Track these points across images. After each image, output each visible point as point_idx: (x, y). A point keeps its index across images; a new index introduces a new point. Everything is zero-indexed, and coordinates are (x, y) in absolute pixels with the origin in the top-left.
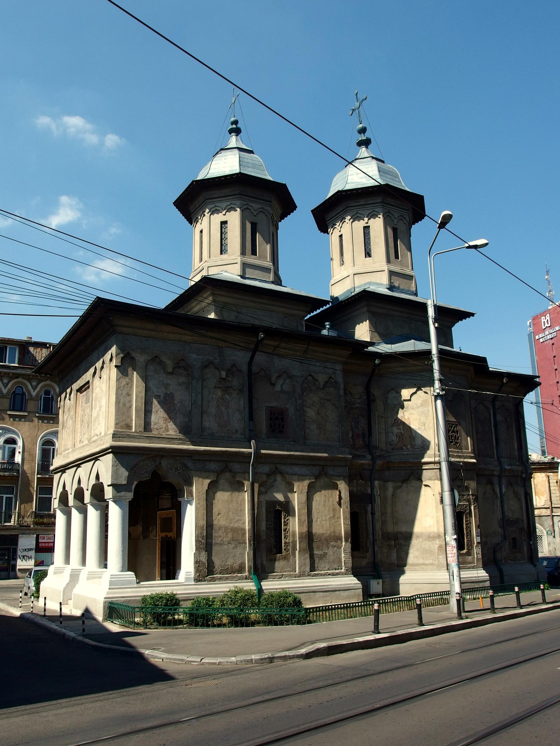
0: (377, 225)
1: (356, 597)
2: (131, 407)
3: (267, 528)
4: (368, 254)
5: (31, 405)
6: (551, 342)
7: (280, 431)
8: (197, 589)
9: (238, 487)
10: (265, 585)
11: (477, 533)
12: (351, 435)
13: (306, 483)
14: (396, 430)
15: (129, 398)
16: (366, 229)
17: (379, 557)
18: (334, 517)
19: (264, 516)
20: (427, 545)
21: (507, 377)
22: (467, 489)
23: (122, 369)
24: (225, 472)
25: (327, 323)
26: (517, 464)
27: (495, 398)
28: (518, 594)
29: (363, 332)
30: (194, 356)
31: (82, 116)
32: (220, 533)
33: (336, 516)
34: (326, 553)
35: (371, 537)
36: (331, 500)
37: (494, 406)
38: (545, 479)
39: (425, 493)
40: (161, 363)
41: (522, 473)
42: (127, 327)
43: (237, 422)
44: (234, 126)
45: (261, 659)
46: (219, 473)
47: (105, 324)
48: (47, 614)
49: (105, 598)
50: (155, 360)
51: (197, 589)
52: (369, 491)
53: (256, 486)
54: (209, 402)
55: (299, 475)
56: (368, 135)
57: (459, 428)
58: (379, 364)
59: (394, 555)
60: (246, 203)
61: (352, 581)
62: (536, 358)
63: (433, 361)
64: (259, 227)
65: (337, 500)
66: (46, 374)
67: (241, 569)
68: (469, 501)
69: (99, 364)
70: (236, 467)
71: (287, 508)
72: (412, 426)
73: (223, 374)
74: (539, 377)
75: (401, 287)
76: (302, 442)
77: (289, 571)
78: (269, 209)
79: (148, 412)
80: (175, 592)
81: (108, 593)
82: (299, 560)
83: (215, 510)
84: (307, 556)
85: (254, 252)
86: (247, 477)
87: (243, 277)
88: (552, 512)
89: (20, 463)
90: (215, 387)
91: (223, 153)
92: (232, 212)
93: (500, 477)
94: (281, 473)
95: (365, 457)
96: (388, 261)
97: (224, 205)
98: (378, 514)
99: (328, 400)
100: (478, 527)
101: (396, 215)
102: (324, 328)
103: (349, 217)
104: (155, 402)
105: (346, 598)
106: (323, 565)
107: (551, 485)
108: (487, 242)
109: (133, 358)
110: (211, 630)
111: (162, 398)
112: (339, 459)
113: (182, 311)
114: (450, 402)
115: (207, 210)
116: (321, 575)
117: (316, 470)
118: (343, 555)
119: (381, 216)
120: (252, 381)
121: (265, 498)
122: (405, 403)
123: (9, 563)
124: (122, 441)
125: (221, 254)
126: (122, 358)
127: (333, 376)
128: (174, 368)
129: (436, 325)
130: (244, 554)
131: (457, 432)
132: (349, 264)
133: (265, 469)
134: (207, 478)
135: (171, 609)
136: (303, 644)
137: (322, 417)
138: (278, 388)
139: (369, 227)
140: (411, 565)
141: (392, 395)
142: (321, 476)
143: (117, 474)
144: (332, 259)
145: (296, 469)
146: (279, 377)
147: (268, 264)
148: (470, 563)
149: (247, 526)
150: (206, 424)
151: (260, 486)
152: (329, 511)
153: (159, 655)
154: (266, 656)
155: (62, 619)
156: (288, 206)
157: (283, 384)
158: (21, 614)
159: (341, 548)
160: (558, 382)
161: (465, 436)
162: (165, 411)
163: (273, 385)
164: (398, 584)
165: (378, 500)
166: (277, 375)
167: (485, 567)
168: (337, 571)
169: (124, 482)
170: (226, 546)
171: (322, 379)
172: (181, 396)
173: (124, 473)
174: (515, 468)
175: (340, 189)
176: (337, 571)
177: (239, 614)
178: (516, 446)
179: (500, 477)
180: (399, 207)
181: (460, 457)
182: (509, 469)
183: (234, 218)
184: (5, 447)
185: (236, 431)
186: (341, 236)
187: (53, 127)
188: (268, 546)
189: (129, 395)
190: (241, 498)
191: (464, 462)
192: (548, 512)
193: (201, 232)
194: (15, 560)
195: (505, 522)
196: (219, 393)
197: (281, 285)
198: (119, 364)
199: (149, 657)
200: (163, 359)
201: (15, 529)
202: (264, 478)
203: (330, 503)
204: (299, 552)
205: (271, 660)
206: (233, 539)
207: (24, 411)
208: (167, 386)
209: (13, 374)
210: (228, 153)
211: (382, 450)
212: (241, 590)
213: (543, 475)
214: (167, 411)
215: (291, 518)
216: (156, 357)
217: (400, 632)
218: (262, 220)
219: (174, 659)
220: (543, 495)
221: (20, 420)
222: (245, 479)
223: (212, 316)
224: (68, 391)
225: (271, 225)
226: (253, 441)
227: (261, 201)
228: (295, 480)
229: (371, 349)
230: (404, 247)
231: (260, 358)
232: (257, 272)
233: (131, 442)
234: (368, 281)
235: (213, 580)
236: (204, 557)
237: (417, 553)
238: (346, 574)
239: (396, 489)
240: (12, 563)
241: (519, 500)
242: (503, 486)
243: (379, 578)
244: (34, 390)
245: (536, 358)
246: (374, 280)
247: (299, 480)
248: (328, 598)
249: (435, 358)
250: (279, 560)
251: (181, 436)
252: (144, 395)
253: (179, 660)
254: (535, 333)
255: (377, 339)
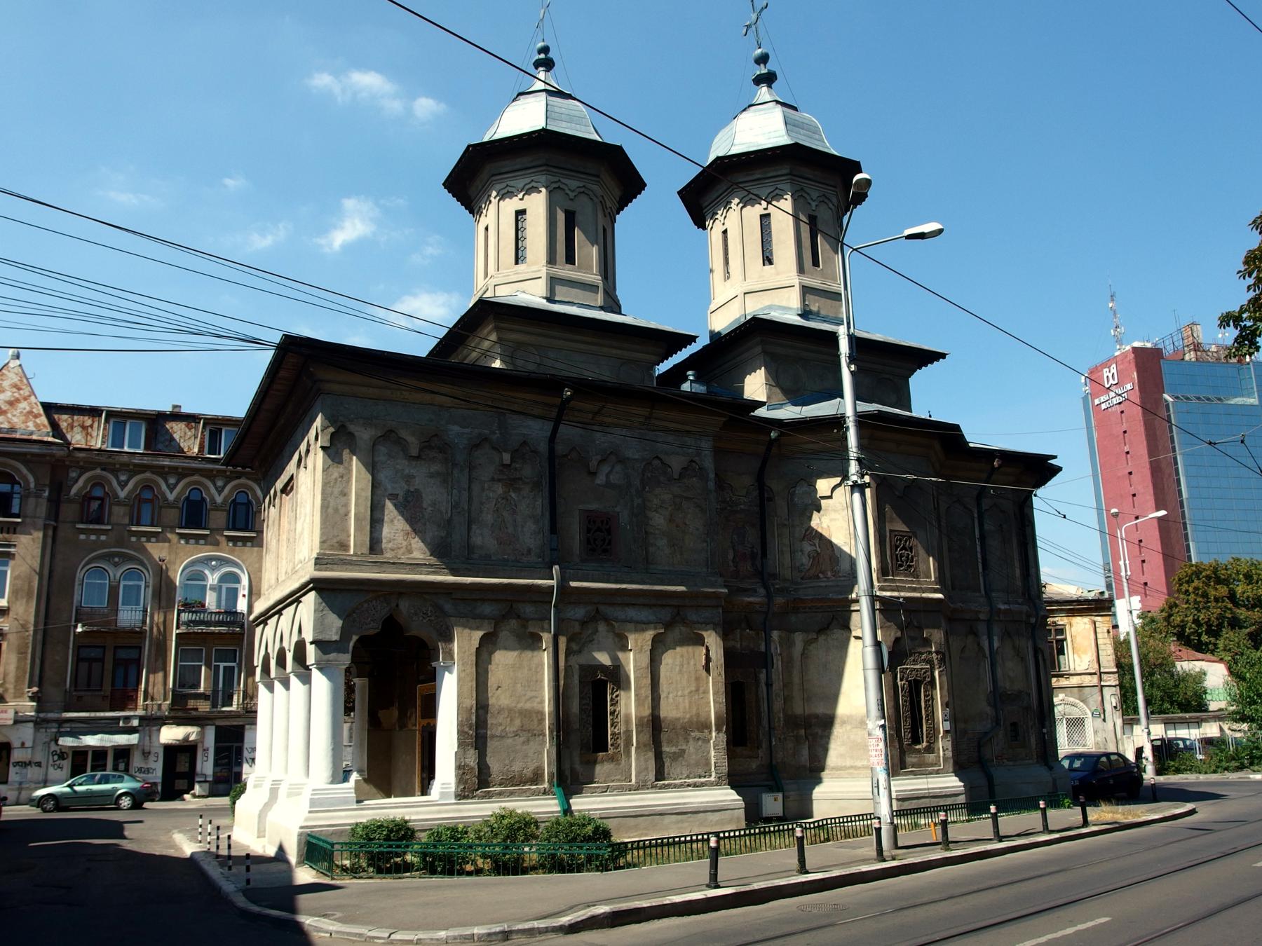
0: (783, 214)
1: (736, 820)
2: (347, 514)
3: (581, 709)
4: (768, 260)
5: (218, 518)
6: (1119, 408)
7: (605, 551)
8: (460, 811)
9: (532, 642)
10: (576, 804)
11: (944, 715)
12: (731, 556)
13: (649, 634)
14: (807, 548)
15: (343, 499)
16: (765, 218)
17: (779, 756)
18: (697, 690)
19: (577, 690)
20: (859, 735)
21: (1000, 458)
22: (927, 642)
23: (333, 452)
24: (508, 619)
25: (690, 373)
26: (1020, 600)
27: (982, 492)
28: (995, 817)
29: (755, 386)
30: (456, 428)
31: (378, 70)
32: (501, 719)
33: (701, 689)
34: (684, 751)
35: (765, 723)
36: (692, 663)
37: (979, 505)
38: (1090, 627)
39: (855, 648)
40: (401, 443)
41: (1029, 616)
42: (340, 383)
43: (530, 536)
44: (542, 56)
45: (489, 935)
46: (499, 621)
47: (307, 377)
48: (233, 853)
49: (302, 828)
50: (389, 436)
51: (460, 811)
52: (763, 648)
53: (563, 641)
54: (482, 503)
55: (637, 622)
56: (771, 66)
57: (914, 542)
58: (776, 439)
59: (805, 752)
60: (556, 179)
61: (728, 796)
62: (1095, 435)
63: (847, 428)
64: (579, 218)
65: (704, 662)
66: (244, 468)
67: (536, 778)
68: (930, 662)
69: (303, 447)
70: (529, 610)
71: (616, 676)
72: (835, 540)
73: (507, 458)
74: (1055, 457)
75: (823, 313)
76: (643, 567)
77: (619, 780)
78: (595, 187)
79: (376, 521)
80: (407, 818)
81: (306, 820)
82: (636, 762)
83: (492, 681)
84: (651, 755)
85: (570, 259)
86: (546, 626)
87: (550, 300)
88: (1101, 680)
89: (245, 611)
90: (493, 479)
91: (524, 100)
92: (534, 195)
93: (989, 623)
94: (607, 620)
95: (755, 591)
96: (801, 270)
97: (520, 183)
98: (776, 687)
99: (687, 499)
100: (946, 705)
101: (815, 195)
102: (685, 379)
103: (736, 200)
104: (389, 505)
105: (717, 823)
106: (678, 770)
107: (1099, 636)
108: (940, 227)
109: (351, 435)
110: (456, 879)
111: (400, 498)
112: (707, 596)
113: (454, 359)
114: (892, 501)
115: (494, 193)
116: (675, 786)
117: (666, 614)
118: (713, 753)
119: (788, 197)
120: (555, 471)
121: (577, 661)
122: (823, 502)
123: (230, 770)
124: (332, 570)
125: (517, 263)
126: (333, 435)
127: (696, 459)
128: (421, 450)
129: (853, 367)
130: (541, 753)
131: (911, 549)
132: (742, 275)
133: (579, 612)
134: (478, 628)
135: (398, 846)
136: (571, 908)
137: (677, 527)
138: (601, 479)
139: (769, 215)
140: (833, 768)
141: (801, 489)
142: (675, 623)
143: (322, 624)
144: (711, 271)
145: (632, 613)
146: (602, 461)
147: (594, 277)
148: (932, 765)
149: (547, 707)
150: (477, 540)
151: (569, 641)
152: (688, 681)
153: (326, 927)
154: (498, 929)
155: (231, 863)
156: (629, 184)
157: (610, 472)
158: (192, 854)
159: (709, 741)
160: (1130, 473)
161: (926, 556)
162: (407, 520)
163: (593, 474)
164: (811, 801)
165: (778, 663)
166: (599, 458)
167: (960, 769)
168: (703, 780)
169: (335, 637)
170: (510, 741)
171: (676, 463)
172: (433, 495)
173: (335, 623)
174: (1015, 607)
175: (721, 155)
176: (703, 780)
177: (507, 851)
178: (1018, 572)
179: (989, 623)
180: (819, 183)
181: (914, 590)
182: (1006, 610)
183: (537, 204)
184: (220, 587)
185: (529, 551)
186: (725, 232)
187: (337, 90)
188: (583, 738)
189: (345, 494)
190: (536, 660)
191: (905, 598)
192: (1094, 680)
193: (487, 229)
194: (240, 765)
195: (999, 698)
196: (499, 489)
197: (620, 313)
198: (327, 444)
199: (310, 929)
200: (404, 434)
201: (239, 716)
202: (577, 628)
203: (692, 668)
204: (637, 748)
205: (506, 935)
206: (522, 729)
207: (251, 531)
208: (409, 478)
209: (183, 468)
210: (530, 98)
211: (785, 580)
212: (512, 813)
213: (1086, 620)
214: (411, 520)
215: (622, 693)
216: (391, 431)
217: (756, 886)
218: (585, 209)
219: (348, 934)
220: (1085, 652)
221: (244, 545)
222: (543, 630)
223: (497, 364)
224: (272, 492)
225: (600, 215)
226: (557, 567)
227: (586, 177)
228: (630, 631)
229: (762, 412)
230: (828, 247)
231: (567, 431)
232: (575, 291)
233: (346, 571)
234: (767, 303)
235: (489, 795)
236: (472, 759)
237: (842, 750)
238: (717, 784)
239: (807, 643)
240: (236, 769)
241: (1023, 659)
242: (995, 638)
243: (778, 791)
244: (218, 494)
245: (1095, 435)
246: (777, 302)
247: (636, 630)
248: (686, 824)
249: (851, 424)
250: (602, 762)
251: (433, 561)
252: (369, 494)
253: (356, 935)
254: (1095, 395)
255: (779, 396)
